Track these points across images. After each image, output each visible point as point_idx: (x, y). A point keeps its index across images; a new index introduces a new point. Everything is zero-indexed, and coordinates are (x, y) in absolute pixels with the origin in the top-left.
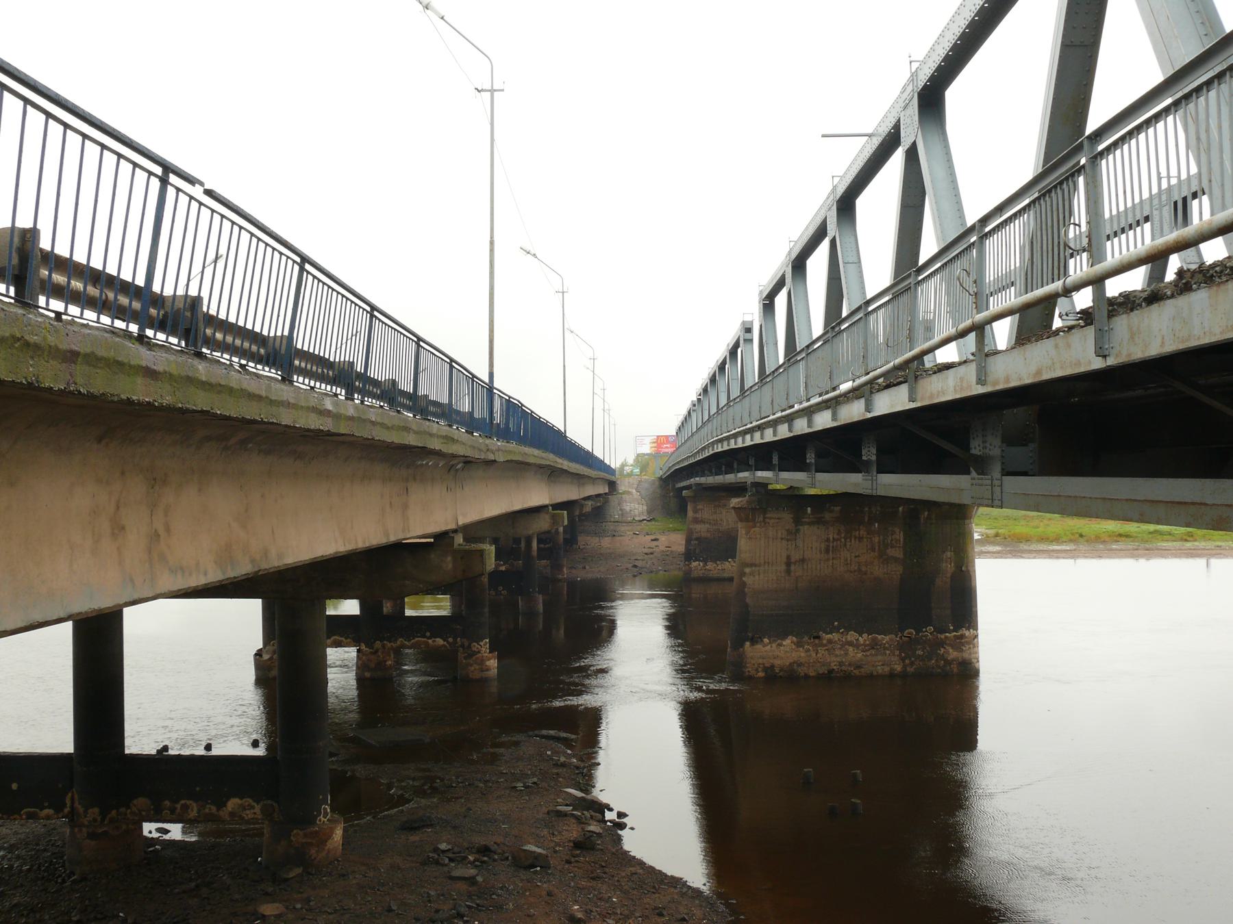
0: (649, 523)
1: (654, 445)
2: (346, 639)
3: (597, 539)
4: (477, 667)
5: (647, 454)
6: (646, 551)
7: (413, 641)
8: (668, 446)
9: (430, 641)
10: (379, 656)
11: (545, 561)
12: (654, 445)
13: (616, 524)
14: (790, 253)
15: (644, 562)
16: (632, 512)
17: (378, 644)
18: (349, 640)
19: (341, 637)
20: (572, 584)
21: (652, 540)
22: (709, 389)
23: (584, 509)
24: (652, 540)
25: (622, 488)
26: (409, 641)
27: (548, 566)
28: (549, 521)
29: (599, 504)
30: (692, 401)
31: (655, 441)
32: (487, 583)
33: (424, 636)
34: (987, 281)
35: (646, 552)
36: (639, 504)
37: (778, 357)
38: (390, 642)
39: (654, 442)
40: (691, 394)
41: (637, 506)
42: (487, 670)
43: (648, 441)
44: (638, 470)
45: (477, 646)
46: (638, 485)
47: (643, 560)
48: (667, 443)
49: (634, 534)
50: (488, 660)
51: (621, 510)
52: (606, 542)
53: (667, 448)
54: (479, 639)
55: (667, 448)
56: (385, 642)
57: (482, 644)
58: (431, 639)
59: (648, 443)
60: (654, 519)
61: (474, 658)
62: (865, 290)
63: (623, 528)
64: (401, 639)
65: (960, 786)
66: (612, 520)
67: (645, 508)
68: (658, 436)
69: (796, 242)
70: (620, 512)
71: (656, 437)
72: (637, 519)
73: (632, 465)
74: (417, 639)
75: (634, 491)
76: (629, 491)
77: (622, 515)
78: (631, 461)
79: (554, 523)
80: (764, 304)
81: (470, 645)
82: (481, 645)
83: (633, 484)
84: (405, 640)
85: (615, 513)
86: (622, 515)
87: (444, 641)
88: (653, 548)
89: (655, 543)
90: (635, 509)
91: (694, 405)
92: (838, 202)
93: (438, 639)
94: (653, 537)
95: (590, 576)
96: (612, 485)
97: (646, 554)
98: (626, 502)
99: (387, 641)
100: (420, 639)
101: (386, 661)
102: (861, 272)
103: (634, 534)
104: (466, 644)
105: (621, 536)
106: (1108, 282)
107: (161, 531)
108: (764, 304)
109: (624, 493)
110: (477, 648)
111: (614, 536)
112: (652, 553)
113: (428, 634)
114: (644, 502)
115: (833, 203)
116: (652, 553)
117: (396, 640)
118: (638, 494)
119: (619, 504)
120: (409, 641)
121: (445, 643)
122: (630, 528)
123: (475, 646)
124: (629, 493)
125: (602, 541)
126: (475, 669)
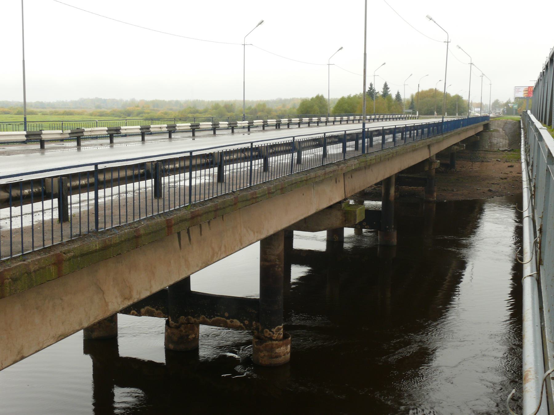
0: (509, 153)
2: (157, 310)
3: (471, 163)
4: (267, 354)
5: (521, 98)
6: (503, 176)
7: (213, 319)
9: (228, 321)
10: (181, 331)
11: (421, 187)
13: (486, 152)
15: (499, 186)
16: (498, 145)
17: (182, 319)
18: (159, 311)
19: (153, 307)
20: (440, 204)
21: (509, 167)
23: (433, 166)
24: (509, 167)
25: (492, 128)
26: (210, 318)
27: (423, 190)
28: (341, 218)
29: (462, 149)
31: (527, 89)
32: (282, 275)
33: (223, 316)
34: (69, 214)
35: (501, 177)
36: (503, 139)
38: (194, 317)
41: (502, 140)
42: (277, 357)
43: (522, 89)
44: (517, 106)
45: (269, 332)
46: (504, 126)
47: (498, 184)
49: (497, 160)
50: (278, 348)
51: (491, 142)
52: (476, 166)
54: (271, 326)
56: (190, 317)
57: (274, 330)
58: (229, 319)
59: (522, 91)
60: (512, 150)
61: (264, 345)
63: (490, 156)
64: (203, 316)
66: (484, 149)
67: (507, 141)
68: (529, 87)
70: (490, 144)
71: (528, 87)
72: (501, 149)
73: (513, 103)
74: (217, 318)
75: (501, 130)
76: (497, 130)
77: (491, 146)
78: (513, 100)
79: (345, 220)
81: (263, 330)
82: (273, 332)
83: (500, 125)
84: (207, 318)
85: (486, 145)
86: (491, 146)
87: (241, 323)
88: (507, 174)
89: (510, 169)
90: (501, 142)
93: (235, 320)
94: (510, 164)
95: (455, 198)
96: (486, 127)
97: (502, 179)
98: (494, 138)
99: (191, 316)
100: (219, 318)
101: (188, 336)
103: (497, 160)
104: (260, 328)
105: (488, 162)
109: (494, 131)
110: (270, 334)
111: (483, 161)
112: (506, 179)
113: (227, 314)
114: (507, 137)
116: (506, 179)
117: (199, 316)
118: (504, 132)
119: (490, 139)
120: (210, 318)
121: (242, 324)
122: (495, 156)
123: (267, 332)
124: (497, 131)
125: (473, 165)
126: (265, 355)
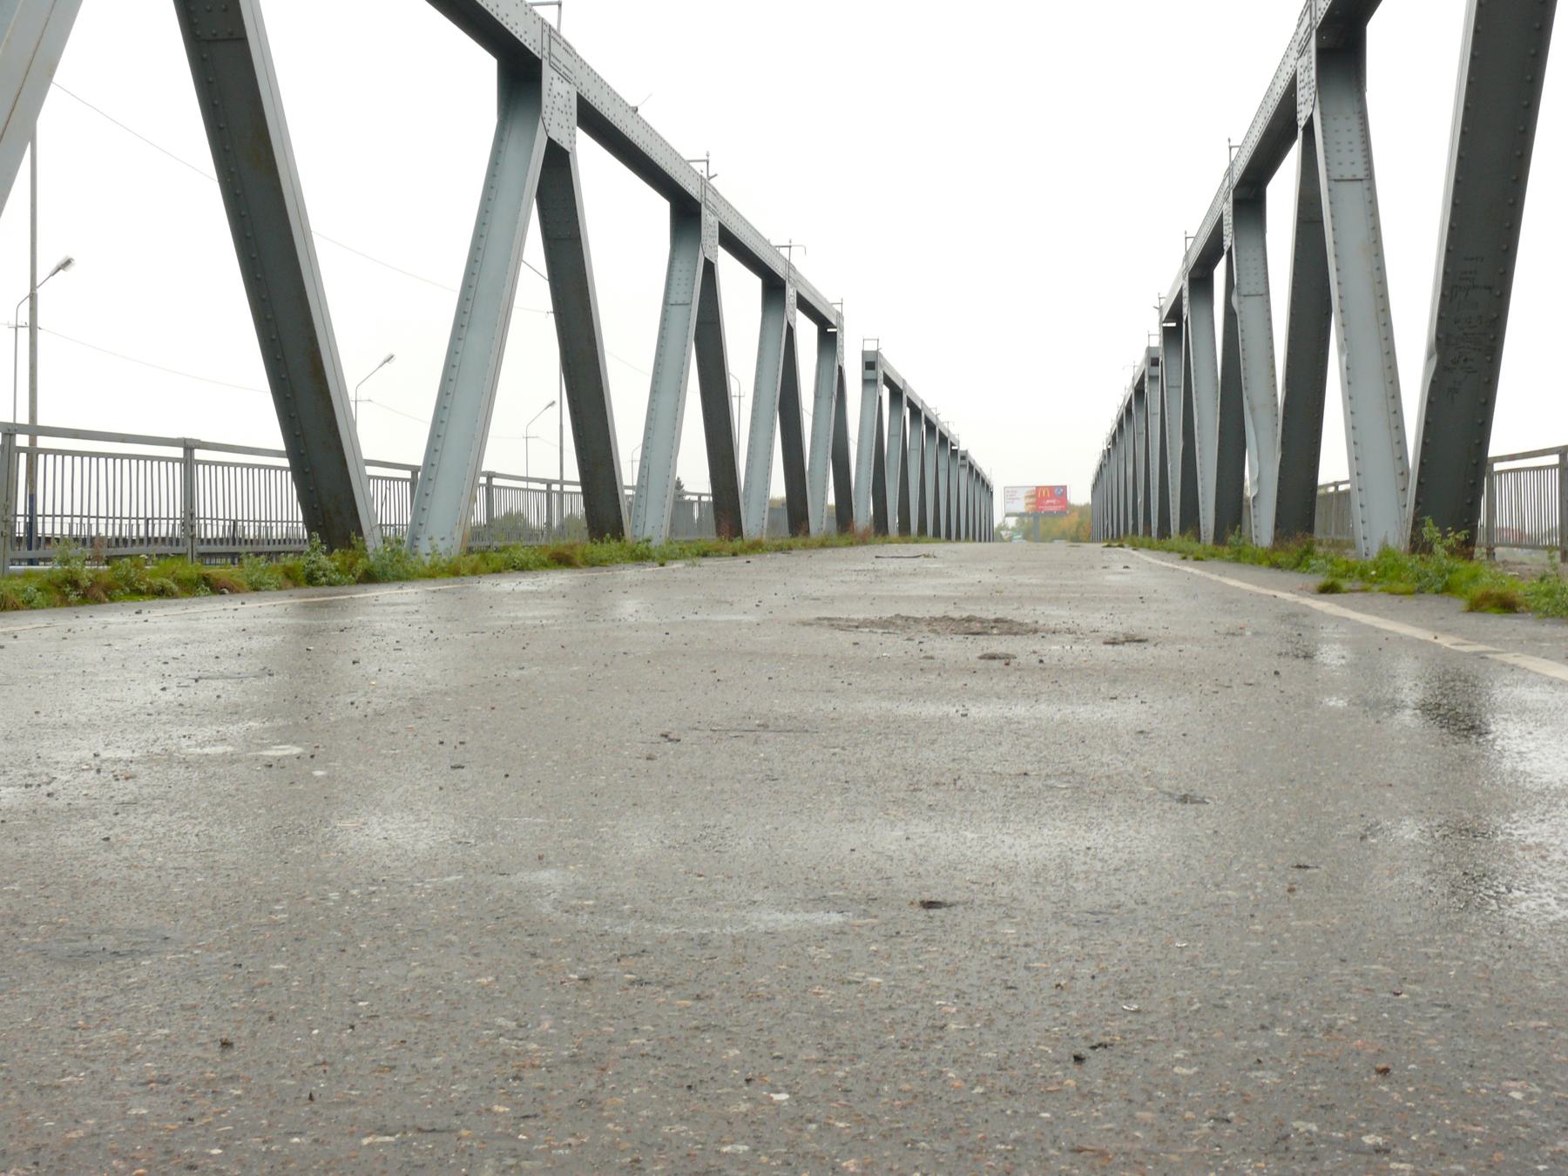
1: (1032, 500)
8: (1054, 501)
12: (1032, 500)
14: (1229, 172)
22: (1185, 310)
30: (1149, 349)
37: (1272, 357)
39: (1031, 497)
40: (1100, 443)
43: (1022, 494)
48: (1051, 498)
53: (1052, 504)
55: (1052, 504)
62: (1274, 361)
65: (1051, 506)
69: (1240, 147)
80: (1165, 329)
91: (1154, 362)
92: (1320, 31)
102: (1373, 202)
106: (494, 479)
107: (1546, 961)
108: (1165, 329)
115: (1310, 34)
